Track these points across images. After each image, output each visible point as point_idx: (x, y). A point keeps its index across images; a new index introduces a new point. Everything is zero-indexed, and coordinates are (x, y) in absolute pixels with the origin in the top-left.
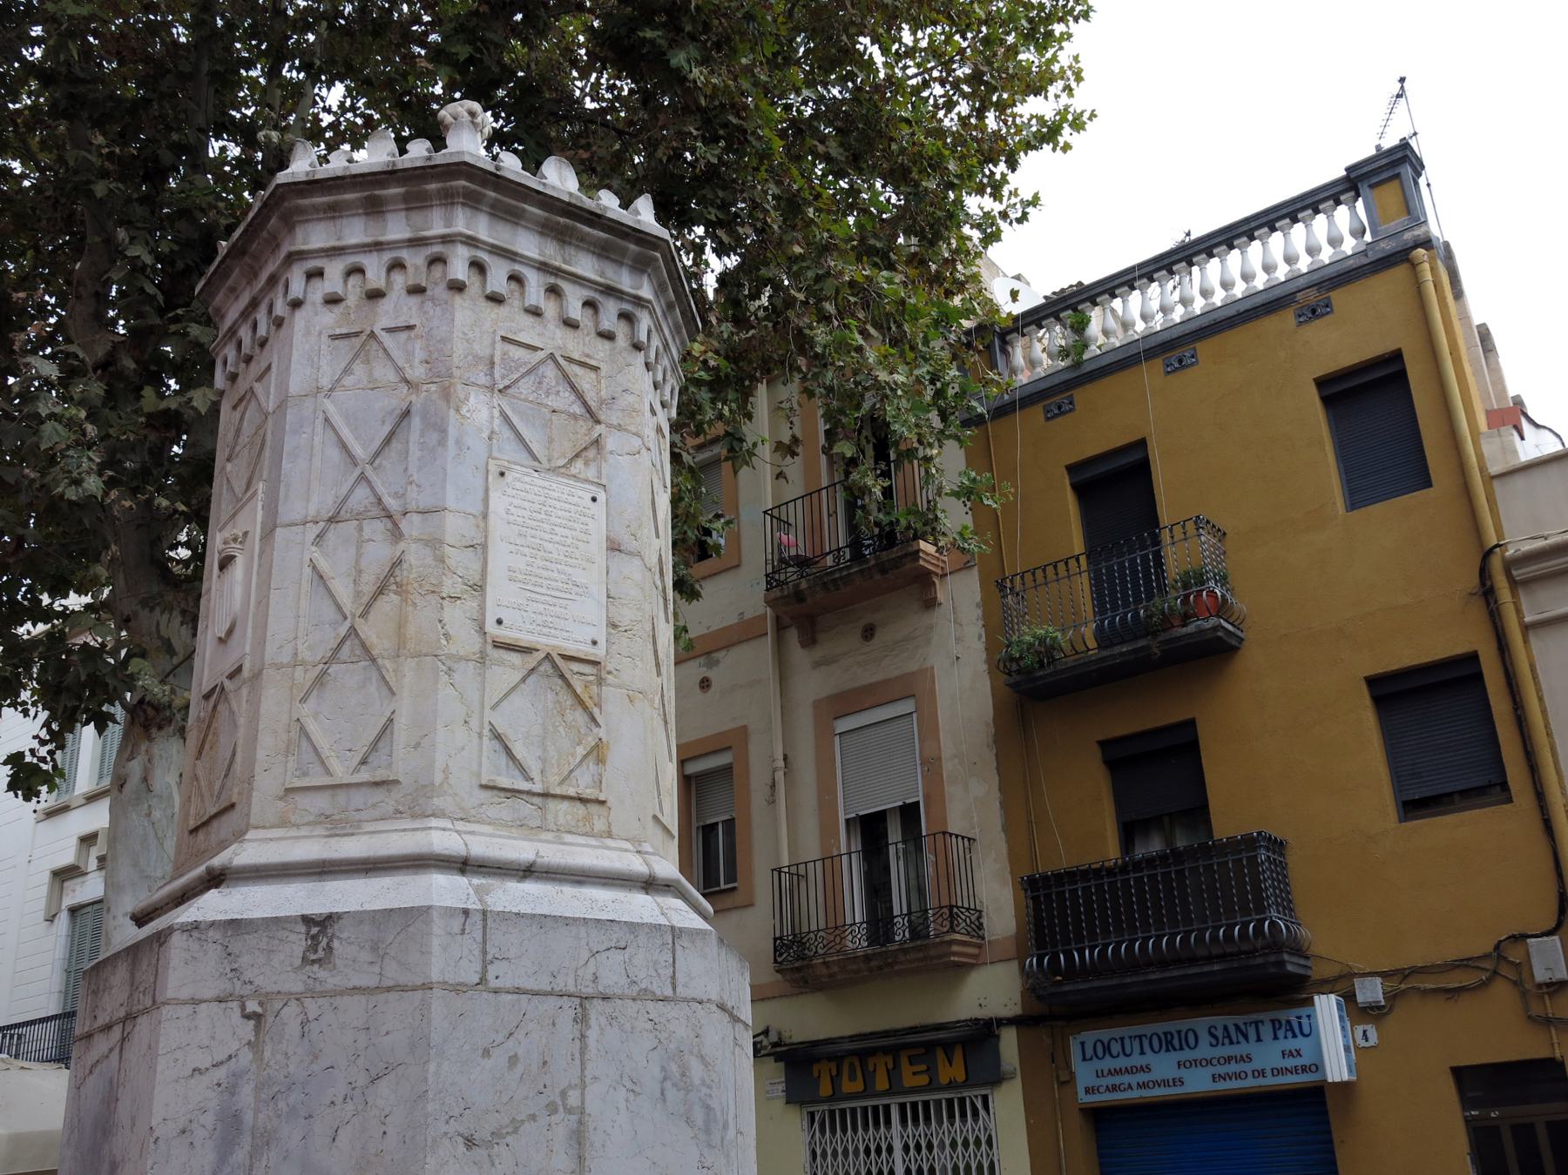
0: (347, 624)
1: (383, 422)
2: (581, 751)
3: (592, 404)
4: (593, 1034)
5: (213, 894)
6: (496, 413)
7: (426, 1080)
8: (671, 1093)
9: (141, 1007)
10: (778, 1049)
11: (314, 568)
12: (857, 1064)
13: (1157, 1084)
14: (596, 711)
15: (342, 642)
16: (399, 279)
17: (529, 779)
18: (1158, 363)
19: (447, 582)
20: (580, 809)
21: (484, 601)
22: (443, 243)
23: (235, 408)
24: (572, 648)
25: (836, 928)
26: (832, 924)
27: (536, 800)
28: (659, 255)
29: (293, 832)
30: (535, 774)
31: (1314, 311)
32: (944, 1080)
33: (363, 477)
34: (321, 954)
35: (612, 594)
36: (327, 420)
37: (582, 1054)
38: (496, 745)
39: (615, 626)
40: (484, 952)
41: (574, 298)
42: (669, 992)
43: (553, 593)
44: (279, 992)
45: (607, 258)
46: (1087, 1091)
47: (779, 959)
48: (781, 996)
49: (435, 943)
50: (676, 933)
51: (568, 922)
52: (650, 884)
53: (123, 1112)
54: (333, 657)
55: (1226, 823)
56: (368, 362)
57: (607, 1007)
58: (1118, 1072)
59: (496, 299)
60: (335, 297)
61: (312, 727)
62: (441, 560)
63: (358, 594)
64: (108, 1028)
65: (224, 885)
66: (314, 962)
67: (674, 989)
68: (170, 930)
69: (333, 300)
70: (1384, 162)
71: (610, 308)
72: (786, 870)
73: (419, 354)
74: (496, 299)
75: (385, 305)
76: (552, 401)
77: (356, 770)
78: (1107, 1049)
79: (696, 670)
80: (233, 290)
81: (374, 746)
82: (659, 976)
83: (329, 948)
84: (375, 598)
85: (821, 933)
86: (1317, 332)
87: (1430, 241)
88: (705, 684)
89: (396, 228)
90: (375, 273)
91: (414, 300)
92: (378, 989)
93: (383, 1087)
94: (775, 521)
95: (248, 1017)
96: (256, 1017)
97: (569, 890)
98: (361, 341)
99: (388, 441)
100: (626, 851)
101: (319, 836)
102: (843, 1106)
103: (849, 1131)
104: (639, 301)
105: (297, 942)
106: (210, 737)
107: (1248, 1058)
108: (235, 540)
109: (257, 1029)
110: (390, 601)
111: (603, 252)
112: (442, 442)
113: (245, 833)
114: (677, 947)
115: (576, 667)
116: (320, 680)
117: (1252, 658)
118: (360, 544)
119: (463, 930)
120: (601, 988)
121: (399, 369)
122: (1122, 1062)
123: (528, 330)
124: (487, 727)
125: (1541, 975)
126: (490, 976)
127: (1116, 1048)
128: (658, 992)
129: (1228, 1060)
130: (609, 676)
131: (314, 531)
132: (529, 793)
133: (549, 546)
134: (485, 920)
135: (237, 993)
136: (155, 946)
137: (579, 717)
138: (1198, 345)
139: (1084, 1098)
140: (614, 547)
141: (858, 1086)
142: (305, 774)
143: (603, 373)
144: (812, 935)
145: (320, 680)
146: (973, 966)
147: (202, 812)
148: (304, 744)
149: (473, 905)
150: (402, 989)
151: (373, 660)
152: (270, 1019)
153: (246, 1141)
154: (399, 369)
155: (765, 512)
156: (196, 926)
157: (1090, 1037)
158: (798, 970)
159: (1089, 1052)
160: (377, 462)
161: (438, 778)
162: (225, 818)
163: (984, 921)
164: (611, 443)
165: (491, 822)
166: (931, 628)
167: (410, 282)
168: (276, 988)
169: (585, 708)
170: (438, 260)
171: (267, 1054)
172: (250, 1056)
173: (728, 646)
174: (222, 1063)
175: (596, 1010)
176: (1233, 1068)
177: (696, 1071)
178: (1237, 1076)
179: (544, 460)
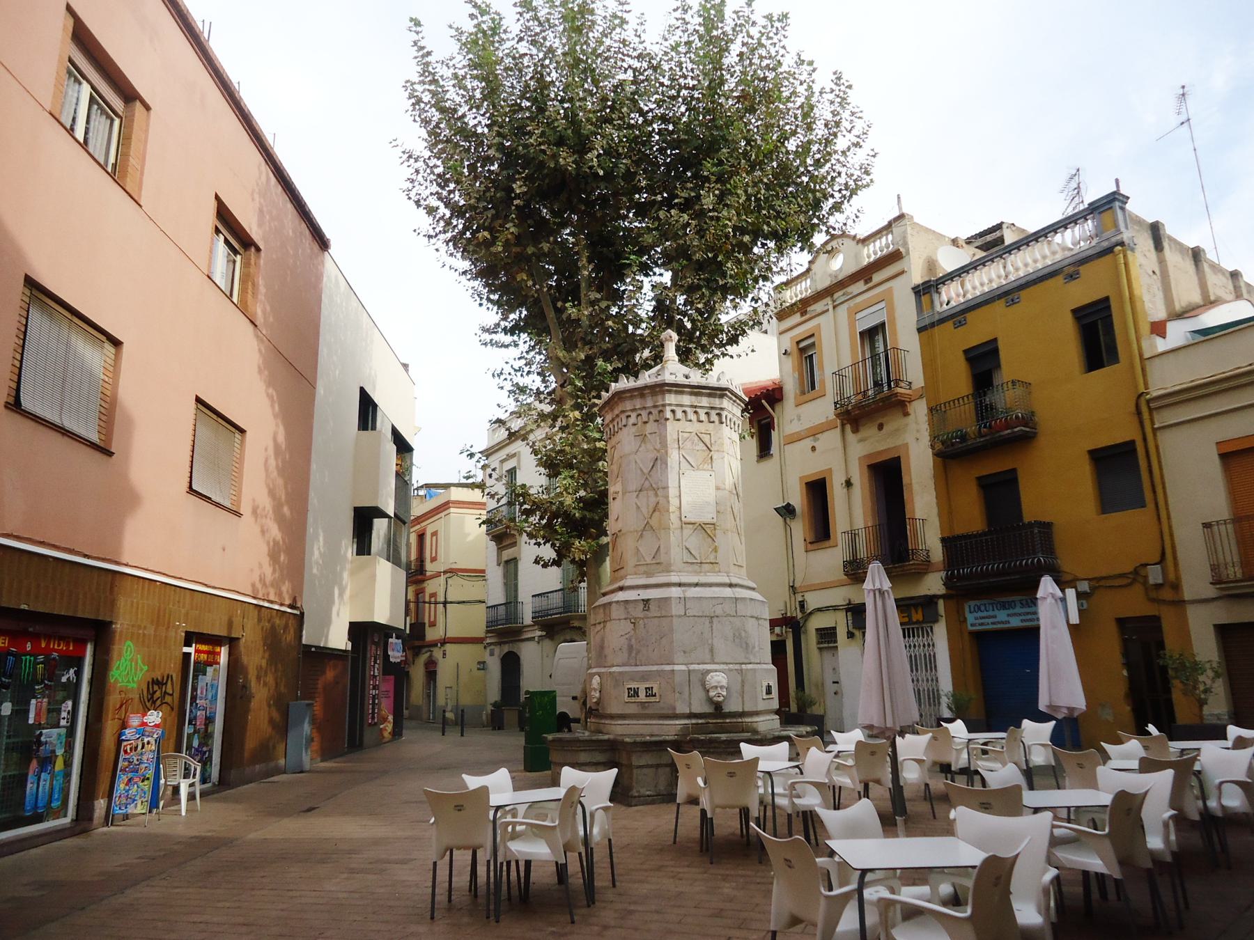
8: (737, 640)
13: (999, 623)
16: (651, 417)
29: (638, 576)
31: (1071, 276)
32: (914, 620)
33: (647, 478)
41: (702, 412)
46: (972, 625)
49: (673, 606)
57: (718, 619)
58: (983, 618)
61: (640, 549)
63: (648, 512)
64: (600, 623)
68: (610, 603)
70: (1105, 201)
71: (713, 413)
76: (697, 448)
78: (979, 609)
86: (1074, 287)
87: (1123, 242)
88: (813, 448)
89: (649, 403)
91: (656, 424)
96: (634, 623)
97: (708, 589)
104: (722, 409)
105: (641, 606)
110: (656, 514)
111: (709, 395)
116: (641, 536)
118: (648, 497)
122: (985, 614)
125: (1151, 581)
127: (983, 608)
129: (1028, 613)
131: (635, 494)
138: (1021, 292)
145: (641, 536)
146: (926, 573)
149: (682, 596)
156: (617, 602)
157: (972, 603)
158: (853, 574)
159: (972, 610)
161: (672, 562)
163: (930, 554)
164: (714, 458)
165: (687, 572)
170: (661, 411)
175: (715, 620)
177: (743, 634)
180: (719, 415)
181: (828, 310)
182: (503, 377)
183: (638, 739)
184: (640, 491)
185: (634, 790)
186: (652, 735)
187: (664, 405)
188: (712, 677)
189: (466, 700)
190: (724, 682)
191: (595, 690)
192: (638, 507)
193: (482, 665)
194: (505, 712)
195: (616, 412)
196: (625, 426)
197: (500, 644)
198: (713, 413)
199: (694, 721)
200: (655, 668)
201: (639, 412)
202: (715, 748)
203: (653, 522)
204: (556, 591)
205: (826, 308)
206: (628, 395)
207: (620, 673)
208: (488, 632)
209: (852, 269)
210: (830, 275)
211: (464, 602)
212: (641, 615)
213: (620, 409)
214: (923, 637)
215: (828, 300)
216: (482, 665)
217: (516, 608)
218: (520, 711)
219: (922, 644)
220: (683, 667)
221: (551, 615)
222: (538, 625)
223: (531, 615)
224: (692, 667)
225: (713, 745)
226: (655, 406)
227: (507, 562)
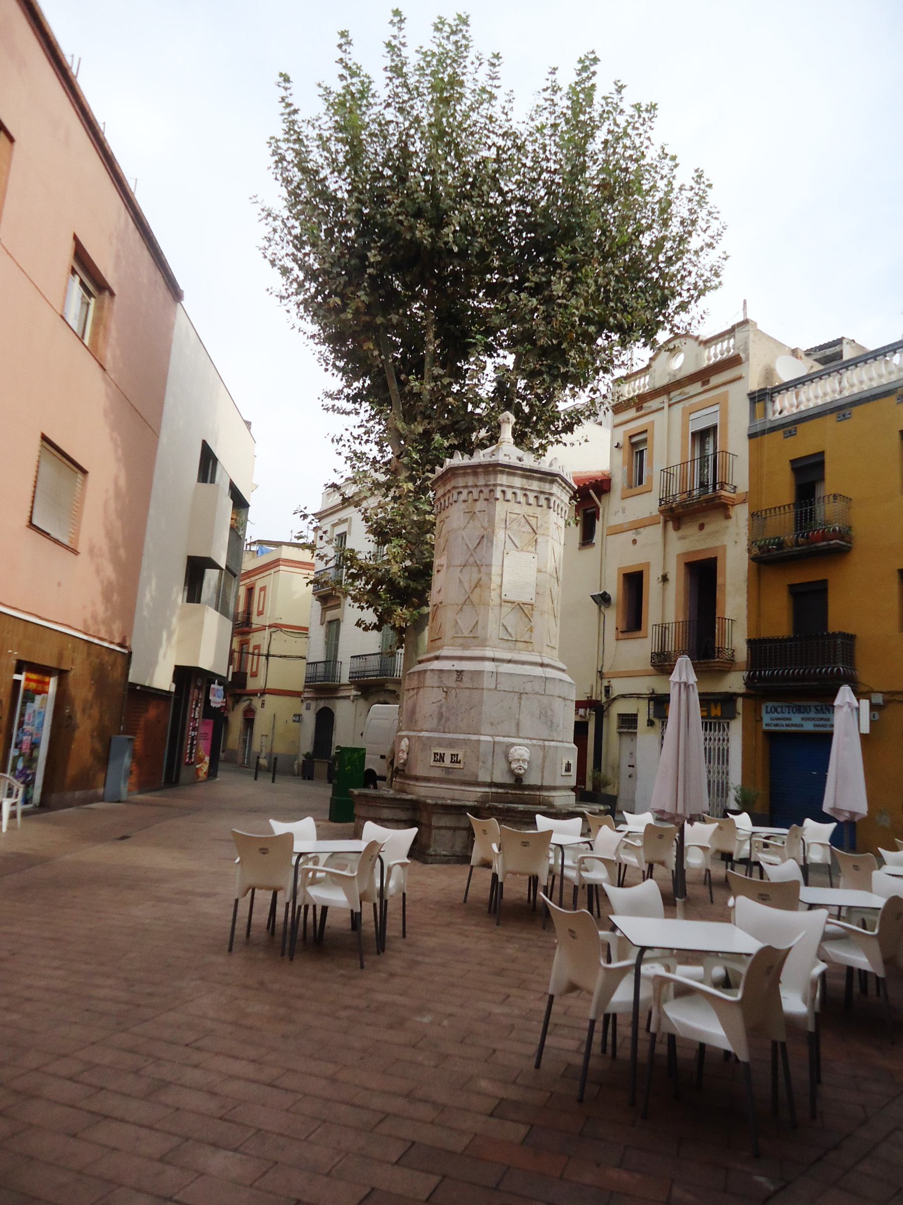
4: (522, 702)
5: (436, 662)
8: (542, 718)
13: (793, 725)
16: (481, 495)
18: (834, 416)
24: (525, 601)
32: (713, 715)
41: (531, 496)
51: (518, 675)
53: (418, 709)
54: (464, 604)
55: (834, 626)
58: (779, 719)
62: (490, 579)
64: (413, 689)
68: (425, 671)
69: (465, 501)
74: (508, 501)
75: (478, 503)
76: (523, 529)
78: (776, 710)
88: (634, 542)
89: (481, 481)
93: (473, 710)
96: (446, 692)
97: (520, 666)
98: (471, 514)
104: (551, 494)
105: (455, 676)
107: (828, 720)
110: (478, 590)
111: (540, 480)
116: (461, 609)
117: (856, 557)
122: (781, 716)
123: (517, 509)
127: (779, 710)
137: (526, 620)
139: (765, 727)
145: (461, 609)
149: (494, 670)
153: (444, 719)
157: (770, 704)
164: (539, 540)
166: (727, 527)
170: (491, 491)
173: (644, 526)
175: (524, 696)
176: (822, 722)
177: (549, 712)
178: (823, 726)
180: (548, 499)
181: (663, 408)
182: (341, 443)
183: (440, 802)
186: (453, 800)
189: (280, 748)
191: (403, 751)
192: (461, 581)
193: (298, 718)
194: (316, 764)
196: (455, 502)
197: (316, 699)
198: (542, 497)
199: (494, 790)
200: (462, 736)
201: (471, 489)
203: (475, 597)
205: (661, 406)
206: (462, 471)
207: (428, 738)
208: (306, 687)
209: (691, 370)
210: (669, 374)
211: (285, 656)
212: (454, 685)
215: (664, 398)
216: (298, 718)
217: (335, 667)
218: (329, 764)
220: (489, 738)
221: (368, 676)
224: (497, 739)
226: (486, 485)
227: (330, 622)
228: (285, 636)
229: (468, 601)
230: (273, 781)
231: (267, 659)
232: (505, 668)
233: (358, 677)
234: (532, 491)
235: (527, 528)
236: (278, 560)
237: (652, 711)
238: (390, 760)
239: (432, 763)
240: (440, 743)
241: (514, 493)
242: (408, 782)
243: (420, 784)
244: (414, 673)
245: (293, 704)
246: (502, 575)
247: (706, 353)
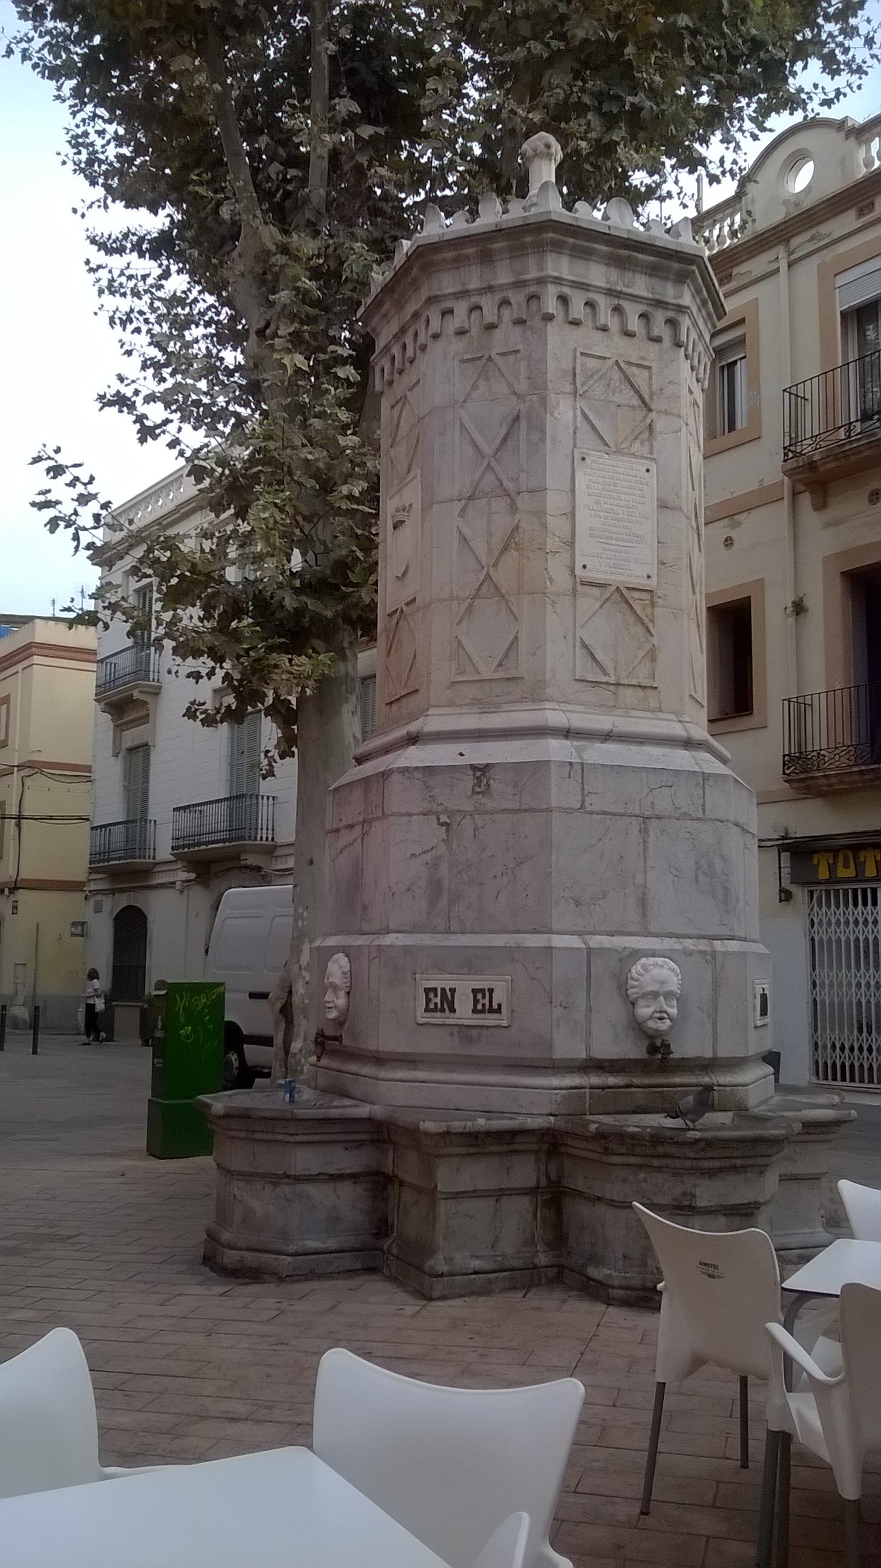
0: (485, 572)
1: (501, 425)
2: (641, 654)
3: (646, 396)
4: (651, 840)
6: (579, 412)
7: (551, 866)
8: (702, 878)
9: (374, 816)
10: (786, 841)
11: (460, 532)
12: (850, 855)
14: (650, 625)
15: (481, 584)
16: (506, 313)
17: (606, 674)
19: (549, 541)
20: (640, 693)
21: (574, 553)
22: (538, 283)
23: (393, 407)
24: (634, 582)
25: (836, 748)
26: (832, 745)
27: (612, 688)
28: (695, 268)
29: (458, 710)
30: (611, 671)
33: (489, 467)
34: (483, 788)
35: (661, 540)
36: (462, 425)
37: (645, 852)
38: (585, 651)
39: (663, 564)
40: (583, 789)
41: (633, 311)
42: (701, 815)
43: (619, 543)
44: (459, 811)
45: (656, 276)
47: (787, 772)
48: (789, 800)
49: (553, 787)
50: (706, 777)
52: (688, 744)
56: (487, 380)
59: (576, 323)
60: (463, 330)
61: (465, 641)
62: (544, 526)
63: (490, 551)
64: (351, 826)
65: (418, 743)
66: (479, 793)
67: (704, 813)
68: (385, 775)
69: (461, 332)
71: (659, 317)
72: (795, 700)
73: (523, 372)
74: (576, 323)
75: (497, 334)
76: (617, 399)
77: (496, 670)
79: (721, 530)
80: (385, 316)
81: (507, 654)
82: (694, 804)
83: (488, 785)
84: (501, 554)
85: (822, 752)
88: (729, 542)
89: (504, 275)
90: (490, 314)
91: (518, 330)
92: (519, 811)
94: (793, 397)
95: (441, 825)
97: (634, 748)
99: (505, 440)
100: (671, 720)
101: (475, 713)
102: (837, 887)
103: (833, 907)
104: (681, 309)
106: (395, 643)
108: (404, 510)
109: (447, 831)
110: (513, 554)
111: (653, 271)
112: (543, 439)
113: (427, 710)
114: (706, 785)
115: (636, 595)
116: (470, 610)
119: (570, 775)
120: (656, 812)
121: (510, 385)
123: (599, 345)
124: (579, 640)
126: (587, 804)
128: (693, 814)
130: (659, 600)
131: (457, 507)
132: (607, 683)
133: (619, 510)
134: (582, 769)
135: (434, 810)
136: (381, 780)
137: (639, 630)
140: (663, 506)
141: (851, 873)
142: (463, 673)
143: (654, 371)
144: (815, 753)
145: (470, 610)
147: (394, 692)
148: (461, 653)
150: (535, 811)
151: (503, 596)
152: (455, 827)
154: (510, 385)
155: (784, 390)
156: (405, 770)
160: (498, 455)
161: (549, 675)
162: (412, 698)
164: (659, 427)
167: (515, 316)
168: (457, 808)
169: (643, 624)
170: (533, 297)
171: (454, 847)
172: (445, 847)
174: (428, 851)
175: (653, 825)
177: (719, 865)
179: (612, 444)
180: (672, 323)
181: (777, 271)
182: (130, 327)
183: (457, 1126)
184: (470, 498)
185: (440, 1256)
186: (488, 1113)
187: (541, 281)
188: (645, 969)
189: (51, 986)
190: (674, 984)
191: (335, 988)
192: (464, 539)
193: (80, 928)
194: (117, 1010)
195: (411, 308)
196: (436, 337)
197: (113, 892)
198: (659, 317)
199: (595, 1080)
200: (501, 940)
201: (475, 300)
202: (666, 1156)
203: (503, 577)
204: (217, 801)
205: (774, 266)
206: (450, 255)
207: (407, 950)
208: (93, 871)
209: (834, 186)
210: (785, 203)
211: (51, 818)
212: (468, 806)
213: (424, 294)
214: (838, 907)
215: (780, 251)
216: (80, 928)
217: (144, 830)
218: (143, 1011)
219: (861, 920)
220: (574, 942)
221: (204, 843)
222: (182, 861)
223: (170, 843)
224: (598, 941)
225: (661, 1150)
226: (519, 284)
227: (131, 750)
228: (51, 783)
229: (488, 588)
230: (35, 1052)
231: (19, 825)
232: (598, 753)
233: (189, 846)
234: (634, 298)
235: (627, 395)
236: (30, 645)
237: (786, 871)
238: (279, 1005)
239: (422, 1017)
240: (440, 961)
241: (590, 304)
242: (353, 1067)
243: (391, 1075)
244: (351, 784)
245: (73, 905)
246: (573, 514)
247: (862, 153)
